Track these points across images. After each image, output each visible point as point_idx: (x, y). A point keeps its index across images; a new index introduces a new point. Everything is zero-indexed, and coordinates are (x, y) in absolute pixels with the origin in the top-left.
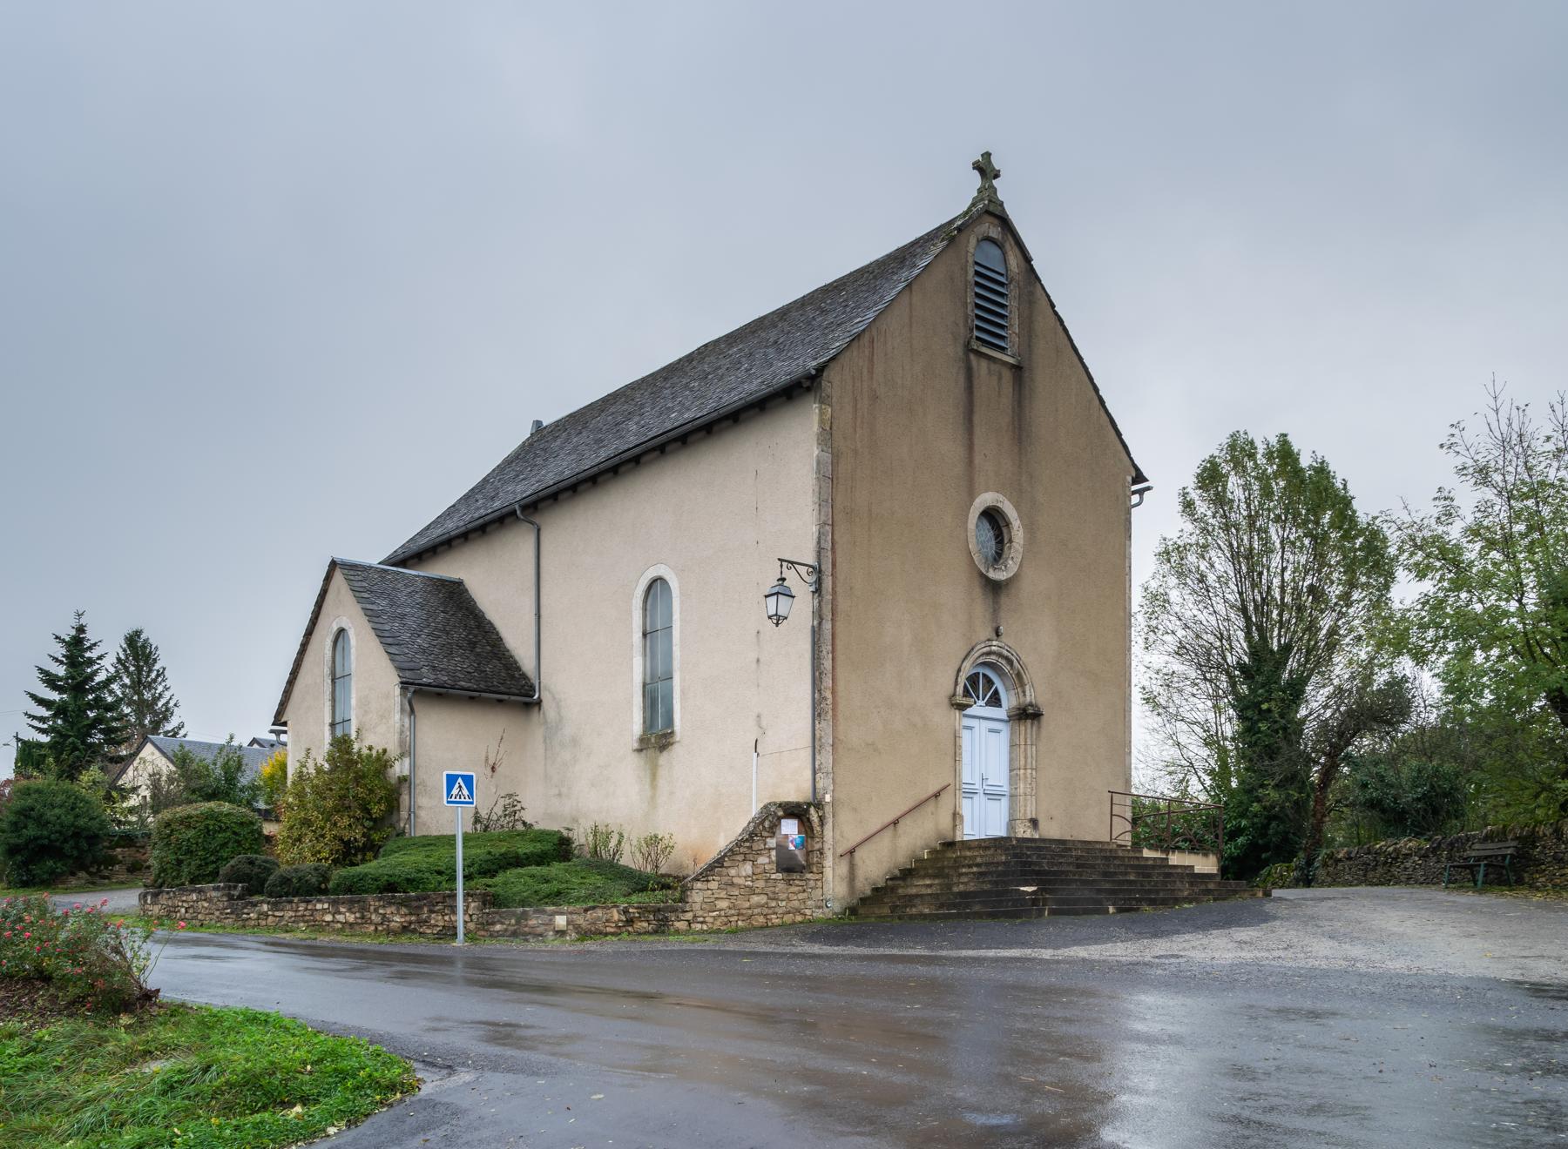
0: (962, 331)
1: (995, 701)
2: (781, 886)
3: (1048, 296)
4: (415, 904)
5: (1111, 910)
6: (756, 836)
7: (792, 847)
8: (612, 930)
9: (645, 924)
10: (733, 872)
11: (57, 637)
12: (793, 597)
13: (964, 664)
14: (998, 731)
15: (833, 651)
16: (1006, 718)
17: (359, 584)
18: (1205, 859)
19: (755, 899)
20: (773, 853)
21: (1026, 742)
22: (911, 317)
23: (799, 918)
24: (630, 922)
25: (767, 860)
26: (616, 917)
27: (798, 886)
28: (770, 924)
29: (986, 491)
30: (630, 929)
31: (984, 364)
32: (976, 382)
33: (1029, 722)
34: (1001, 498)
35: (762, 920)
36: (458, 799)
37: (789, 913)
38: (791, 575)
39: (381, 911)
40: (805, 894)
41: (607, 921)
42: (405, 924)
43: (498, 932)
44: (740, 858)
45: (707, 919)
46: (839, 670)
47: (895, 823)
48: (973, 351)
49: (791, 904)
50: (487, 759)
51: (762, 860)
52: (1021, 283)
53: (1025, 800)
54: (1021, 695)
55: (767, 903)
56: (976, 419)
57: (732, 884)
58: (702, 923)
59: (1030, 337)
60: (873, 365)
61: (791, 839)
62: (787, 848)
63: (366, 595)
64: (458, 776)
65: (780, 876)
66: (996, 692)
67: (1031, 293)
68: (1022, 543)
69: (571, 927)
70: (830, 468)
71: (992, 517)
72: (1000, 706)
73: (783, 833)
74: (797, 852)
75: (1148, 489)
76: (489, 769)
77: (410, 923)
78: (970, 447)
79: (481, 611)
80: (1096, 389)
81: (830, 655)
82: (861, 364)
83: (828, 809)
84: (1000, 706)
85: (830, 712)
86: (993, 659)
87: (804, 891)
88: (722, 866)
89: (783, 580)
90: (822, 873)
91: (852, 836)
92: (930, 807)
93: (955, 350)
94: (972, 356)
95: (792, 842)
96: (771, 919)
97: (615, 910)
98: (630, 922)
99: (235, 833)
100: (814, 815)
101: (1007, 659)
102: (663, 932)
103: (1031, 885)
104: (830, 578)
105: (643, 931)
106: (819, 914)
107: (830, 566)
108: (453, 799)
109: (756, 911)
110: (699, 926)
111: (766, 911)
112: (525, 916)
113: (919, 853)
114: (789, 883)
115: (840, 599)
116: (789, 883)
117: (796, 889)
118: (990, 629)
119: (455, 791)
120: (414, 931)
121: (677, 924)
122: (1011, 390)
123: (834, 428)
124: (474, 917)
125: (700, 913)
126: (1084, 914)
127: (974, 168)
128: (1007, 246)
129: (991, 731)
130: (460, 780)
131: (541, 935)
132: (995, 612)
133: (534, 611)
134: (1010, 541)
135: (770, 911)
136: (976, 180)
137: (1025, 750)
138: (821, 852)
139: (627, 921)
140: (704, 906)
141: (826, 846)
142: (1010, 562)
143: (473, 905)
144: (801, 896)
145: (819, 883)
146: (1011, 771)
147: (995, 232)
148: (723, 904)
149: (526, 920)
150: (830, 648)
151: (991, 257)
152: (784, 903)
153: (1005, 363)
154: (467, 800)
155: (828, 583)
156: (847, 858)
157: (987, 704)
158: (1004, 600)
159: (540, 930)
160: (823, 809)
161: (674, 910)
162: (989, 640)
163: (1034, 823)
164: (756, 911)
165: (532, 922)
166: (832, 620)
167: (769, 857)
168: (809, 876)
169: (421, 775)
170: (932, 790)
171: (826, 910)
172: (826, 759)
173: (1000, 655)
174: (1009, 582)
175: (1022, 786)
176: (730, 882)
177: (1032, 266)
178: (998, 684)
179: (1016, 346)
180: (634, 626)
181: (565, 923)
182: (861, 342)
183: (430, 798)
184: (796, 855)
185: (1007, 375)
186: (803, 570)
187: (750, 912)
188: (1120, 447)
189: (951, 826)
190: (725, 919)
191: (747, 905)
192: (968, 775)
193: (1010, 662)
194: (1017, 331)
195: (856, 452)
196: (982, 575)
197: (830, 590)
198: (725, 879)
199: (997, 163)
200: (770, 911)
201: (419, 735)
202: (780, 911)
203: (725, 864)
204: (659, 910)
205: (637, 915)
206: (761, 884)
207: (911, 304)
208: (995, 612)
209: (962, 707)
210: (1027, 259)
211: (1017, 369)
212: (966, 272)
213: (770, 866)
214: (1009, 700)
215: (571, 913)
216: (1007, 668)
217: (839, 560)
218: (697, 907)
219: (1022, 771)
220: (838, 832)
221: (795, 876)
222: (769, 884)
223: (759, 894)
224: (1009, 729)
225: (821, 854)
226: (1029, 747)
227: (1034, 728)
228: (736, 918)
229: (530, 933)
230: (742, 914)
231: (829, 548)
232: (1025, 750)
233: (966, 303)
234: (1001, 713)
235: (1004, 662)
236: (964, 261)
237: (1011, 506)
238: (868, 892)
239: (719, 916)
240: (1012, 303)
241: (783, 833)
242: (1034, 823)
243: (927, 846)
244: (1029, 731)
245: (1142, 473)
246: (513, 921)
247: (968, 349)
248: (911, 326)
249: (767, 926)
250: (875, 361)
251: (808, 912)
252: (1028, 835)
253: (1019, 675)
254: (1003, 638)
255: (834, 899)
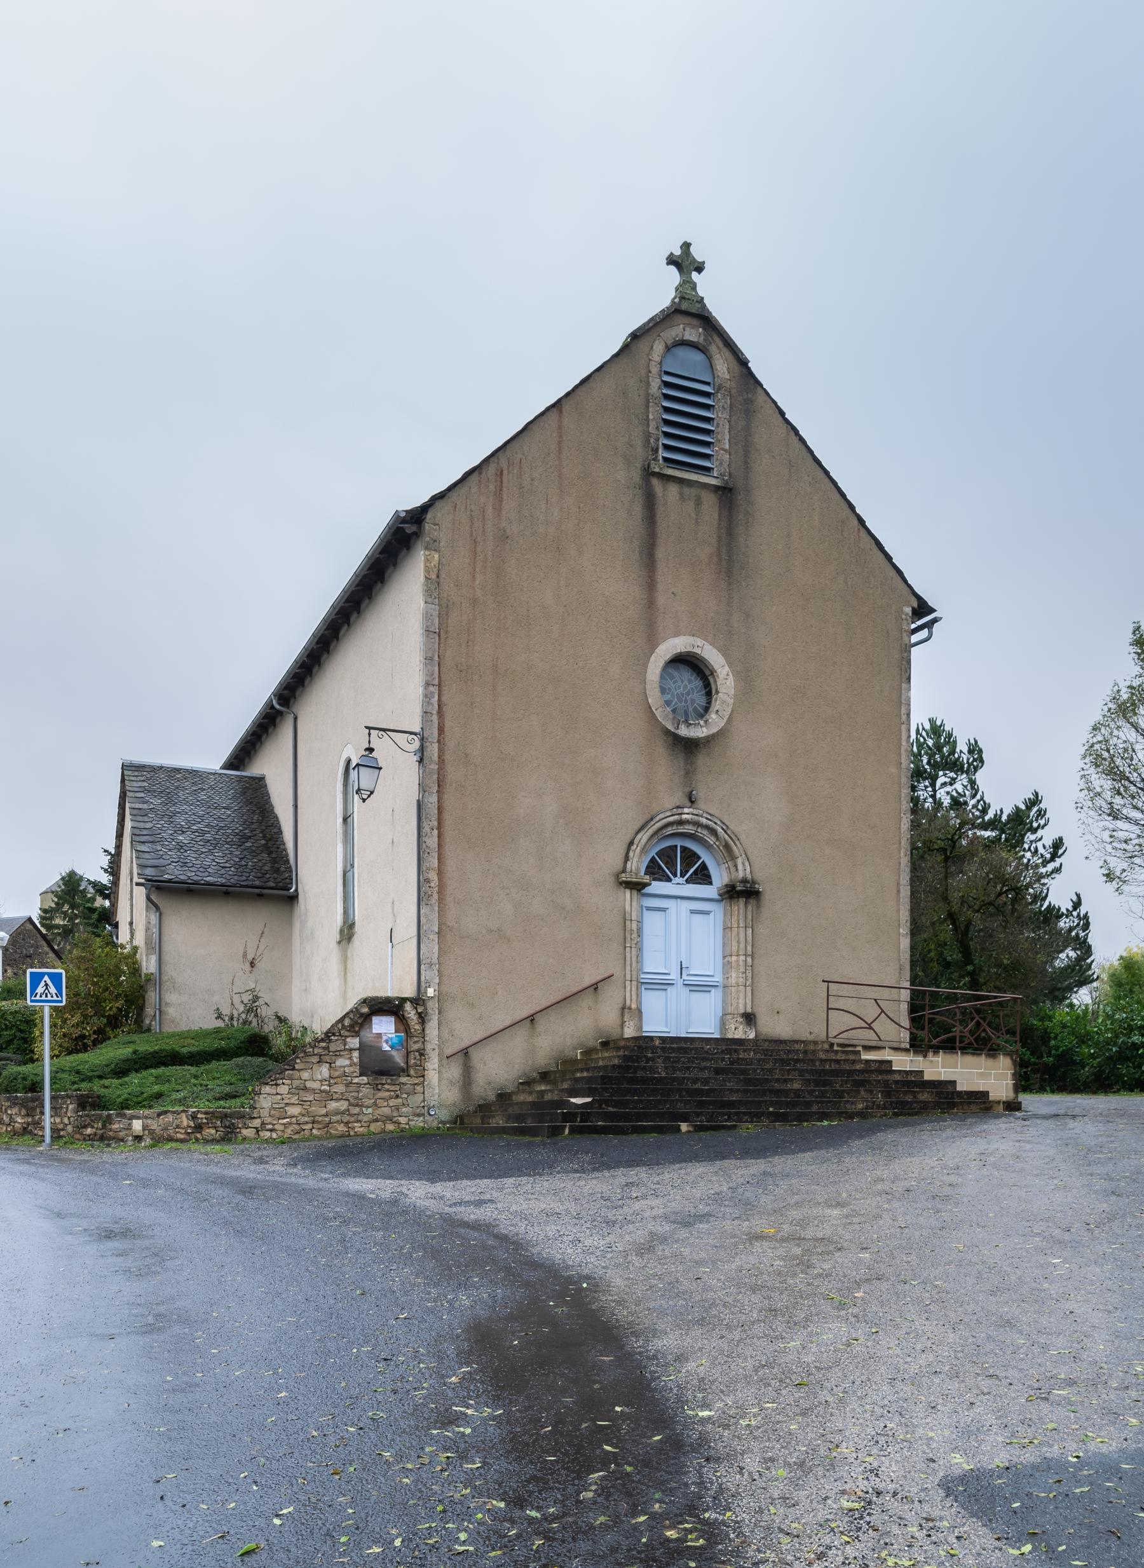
0: (640, 451)
1: (702, 876)
2: (365, 1091)
3: (775, 403)
4: (31, 1104)
5: (684, 1127)
6: (334, 1035)
7: (386, 1048)
8: (182, 1136)
9: (213, 1131)
10: (305, 1075)
11: (105, 851)
12: (380, 768)
13: (639, 837)
14: (707, 913)
15: (440, 826)
16: (716, 896)
17: (140, 784)
18: (990, 1062)
19: (333, 1105)
20: (356, 1054)
21: (738, 924)
22: (560, 443)
23: (390, 1127)
24: (199, 1128)
25: (347, 1062)
26: (185, 1122)
27: (388, 1090)
28: (352, 1133)
29: (676, 635)
30: (198, 1136)
31: (673, 489)
32: (660, 510)
33: (742, 901)
34: (699, 642)
35: (342, 1128)
36: (44, 998)
37: (377, 1120)
38: (384, 748)
39: (9, 1112)
40: (400, 1100)
41: (178, 1127)
42: (25, 1126)
43: (89, 1135)
44: (315, 1059)
45: (276, 1127)
46: (448, 848)
47: (532, 1019)
48: (654, 474)
49: (379, 1111)
50: (245, 955)
51: (341, 1062)
52: (734, 391)
53: (738, 991)
54: (733, 869)
55: (348, 1110)
56: (660, 553)
57: (305, 1089)
58: (271, 1130)
59: (747, 453)
60: (501, 501)
61: (384, 1038)
62: (380, 1049)
63: (142, 795)
64: (44, 974)
65: (365, 1079)
66: (704, 867)
67: (750, 402)
68: (732, 692)
69: (146, 1132)
70: (436, 621)
71: (688, 662)
72: (711, 883)
73: (374, 1031)
74: (394, 1053)
75: (935, 620)
76: (248, 964)
77: (28, 1124)
78: (651, 586)
79: (272, 805)
80: (852, 507)
81: (436, 832)
82: (482, 500)
83: (432, 1006)
84: (711, 883)
85: (436, 896)
86: (688, 829)
87: (397, 1096)
88: (294, 1069)
89: (371, 750)
90: (423, 1076)
91: (466, 1031)
92: (587, 1000)
93: (627, 476)
94: (655, 482)
95: (387, 1042)
96: (354, 1128)
97: (184, 1115)
98: (199, 1128)
99: (21, 1031)
100: (410, 1011)
101: (707, 827)
102: (230, 1140)
103: (583, 1096)
104: (436, 746)
105: (210, 1138)
106: (418, 1123)
107: (436, 732)
108: (38, 998)
109: (334, 1118)
110: (268, 1134)
111: (346, 1118)
112: (108, 1120)
113: (569, 1053)
114: (376, 1087)
115: (449, 768)
116: (376, 1087)
117: (387, 1094)
118: (680, 794)
119: (40, 989)
120: (31, 1133)
121: (245, 1132)
122: (716, 515)
123: (443, 576)
124: (72, 1119)
125: (269, 1120)
126: (633, 1133)
127: (668, 264)
128: (713, 349)
129: (693, 912)
130: (46, 978)
131: (122, 1140)
132: (689, 775)
133: (291, 803)
134: (717, 692)
135: (353, 1119)
136: (673, 276)
137: (738, 934)
138: (422, 1053)
139: (195, 1127)
140: (273, 1112)
141: (428, 1047)
142: (714, 716)
143: (71, 1107)
144: (392, 1103)
145: (419, 1089)
146: (724, 957)
147: (693, 334)
148: (294, 1111)
149: (110, 1124)
150: (436, 823)
151: (688, 363)
152: (370, 1110)
153: (705, 486)
154: (55, 998)
155: (433, 750)
156: (460, 1058)
157: (687, 881)
158: (702, 761)
159: (122, 1134)
160: (424, 1004)
161: (242, 1116)
162: (678, 807)
163: (749, 1018)
164: (334, 1118)
165: (115, 1126)
166: (438, 792)
167: (350, 1058)
168: (404, 1079)
169: (170, 971)
170: (588, 980)
171: (428, 1118)
172: (431, 949)
173: (698, 824)
174: (709, 740)
175: (734, 975)
176: (302, 1086)
177: (749, 369)
178: (705, 857)
179: (726, 465)
180: (338, 812)
181: (141, 1128)
182: (484, 475)
183: (180, 994)
184: (392, 1056)
185: (710, 501)
186: (401, 739)
187: (327, 1119)
188: (893, 573)
189: (618, 1022)
190: (297, 1127)
191: (324, 1111)
192: (654, 963)
193: (713, 832)
194: (727, 447)
195: (474, 602)
196: (668, 732)
197: (436, 758)
198: (296, 1083)
199: (697, 253)
200: (353, 1119)
201: (166, 931)
202: (365, 1119)
203: (297, 1067)
204: (226, 1116)
205: (205, 1121)
206: (340, 1088)
207: (560, 427)
208: (689, 775)
209: (638, 887)
210: (743, 363)
211: (725, 492)
212: (648, 384)
213: (352, 1069)
214: (720, 877)
215: (146, 1118)
216: (711, 840)
217: (448, 724)
218: (265, 1113)
219: (734, 958)
220: (445, 1031)
221: (384, 1079)
222: (351, 1089)
223: (337, 1100)
224: (722, 909)
225: (422, 1055)
226: (742, 930)
227: (750, 908)
228: (310, 1126)
229: (114, 1138)
230: (318, 1122)
231: (435, 712)
232: (738, 934)
233: (647, 419)
234: (710, 891)
235: (705, 832)
236: (643, 372)
237: (715, 651)
238: (492, 1097)
239: (290, 1124)
240: (720, 415)
241: (374, 1031)
242: (749, 1018)
243: (581, 1045)
244: (741, 911)
245: (926, 602)
246: (100, 1125)
247: (648, 474)
248: (560, 452)
249: (349, 1135)
250: (505, 496)
251: (403, 1120)
252: (739, 1035)
253: (727, 847)
254: (701, 804)
255: (441, 1106)
